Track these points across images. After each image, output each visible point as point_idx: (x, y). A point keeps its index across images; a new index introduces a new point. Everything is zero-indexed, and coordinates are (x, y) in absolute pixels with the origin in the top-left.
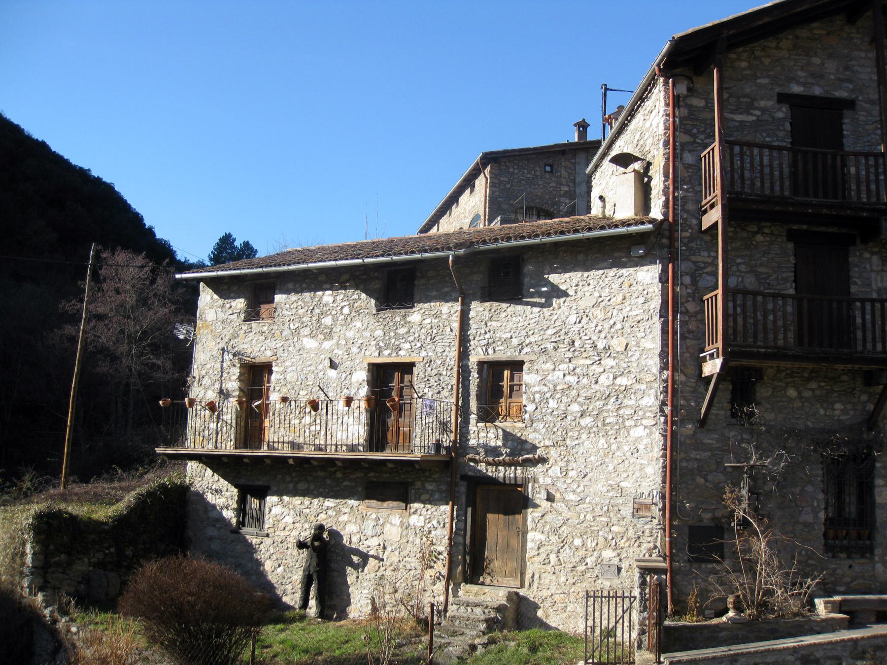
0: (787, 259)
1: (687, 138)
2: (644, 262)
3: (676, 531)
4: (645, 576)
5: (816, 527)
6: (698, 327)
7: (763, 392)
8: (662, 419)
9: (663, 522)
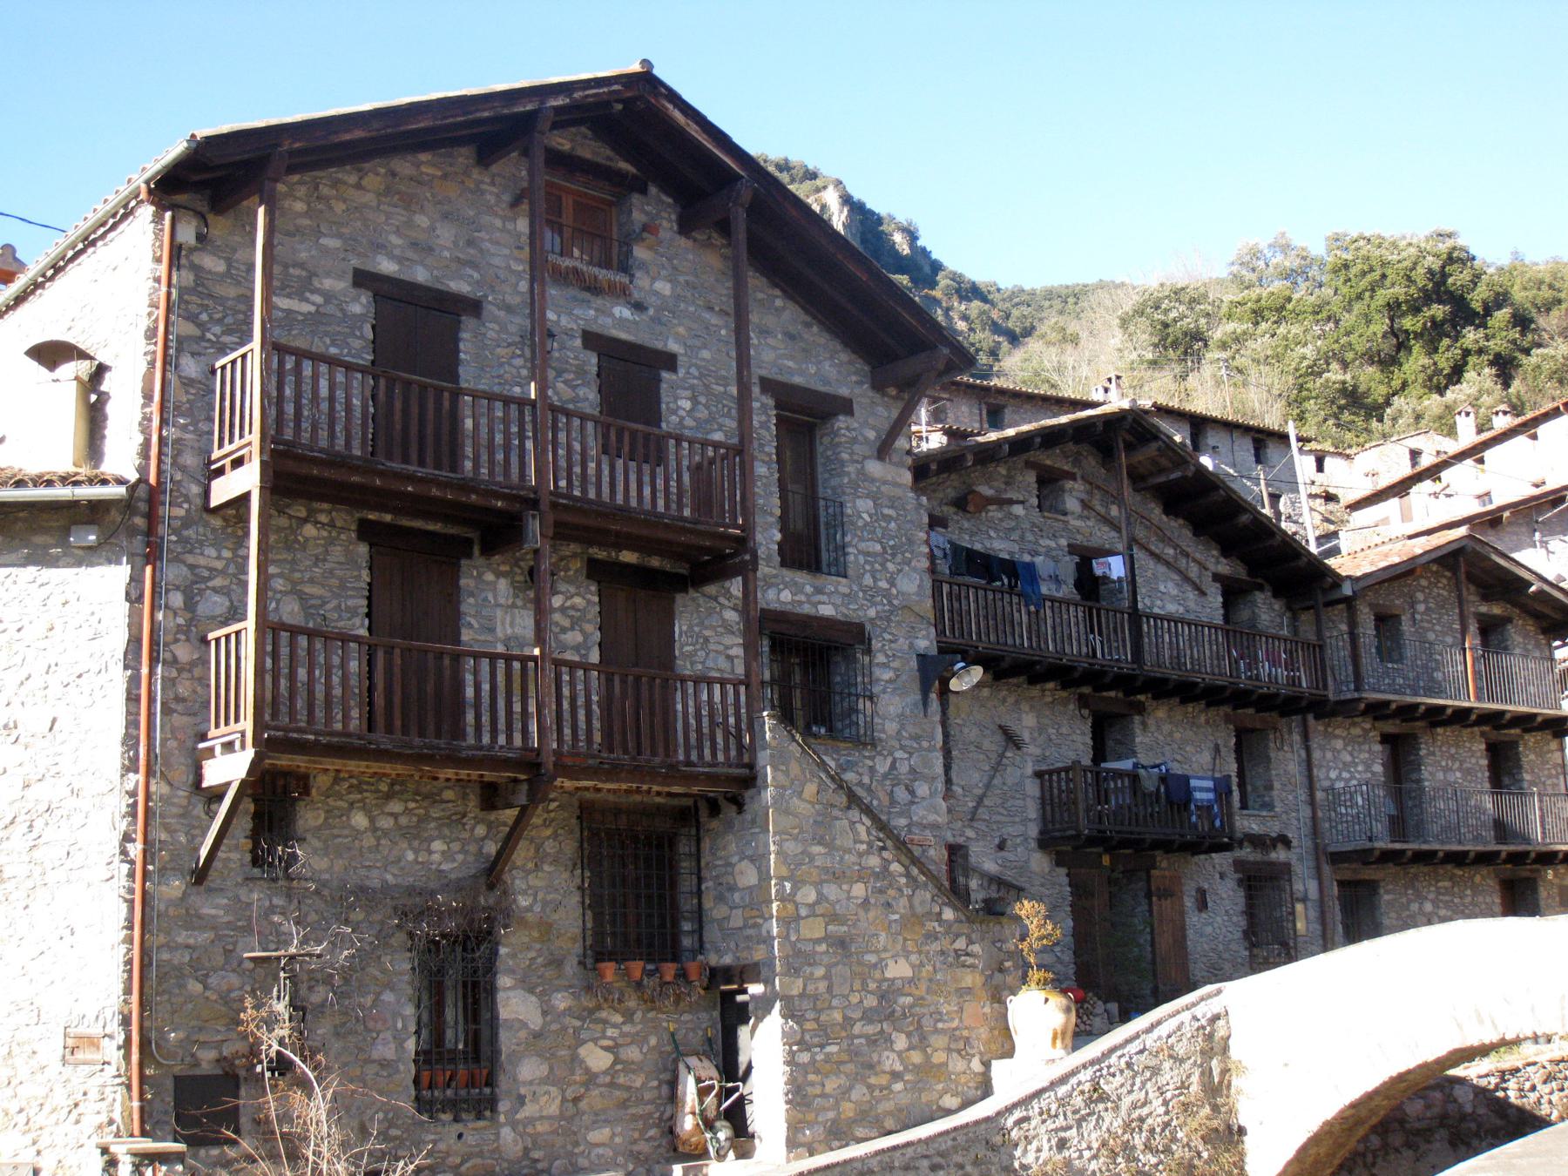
0: (355, 573)
1: (189, 329)
2: (94, 560)
3: (151, 1088)
4: (143, 1169)
5: (402, 1068)
6: (195, 692)
7: (308, 818)
8: (125, 867)
9: (127, 1070)
